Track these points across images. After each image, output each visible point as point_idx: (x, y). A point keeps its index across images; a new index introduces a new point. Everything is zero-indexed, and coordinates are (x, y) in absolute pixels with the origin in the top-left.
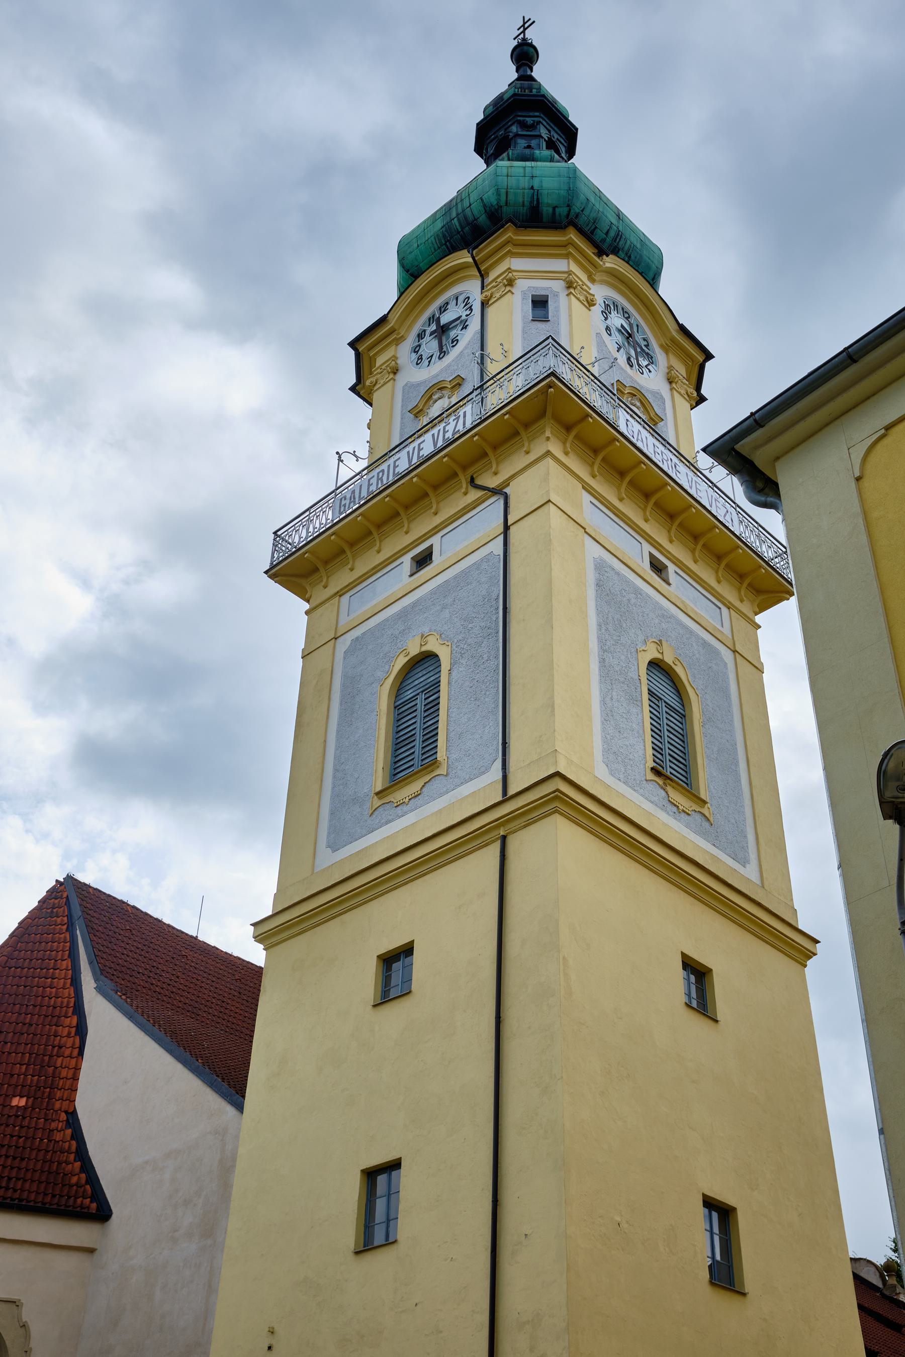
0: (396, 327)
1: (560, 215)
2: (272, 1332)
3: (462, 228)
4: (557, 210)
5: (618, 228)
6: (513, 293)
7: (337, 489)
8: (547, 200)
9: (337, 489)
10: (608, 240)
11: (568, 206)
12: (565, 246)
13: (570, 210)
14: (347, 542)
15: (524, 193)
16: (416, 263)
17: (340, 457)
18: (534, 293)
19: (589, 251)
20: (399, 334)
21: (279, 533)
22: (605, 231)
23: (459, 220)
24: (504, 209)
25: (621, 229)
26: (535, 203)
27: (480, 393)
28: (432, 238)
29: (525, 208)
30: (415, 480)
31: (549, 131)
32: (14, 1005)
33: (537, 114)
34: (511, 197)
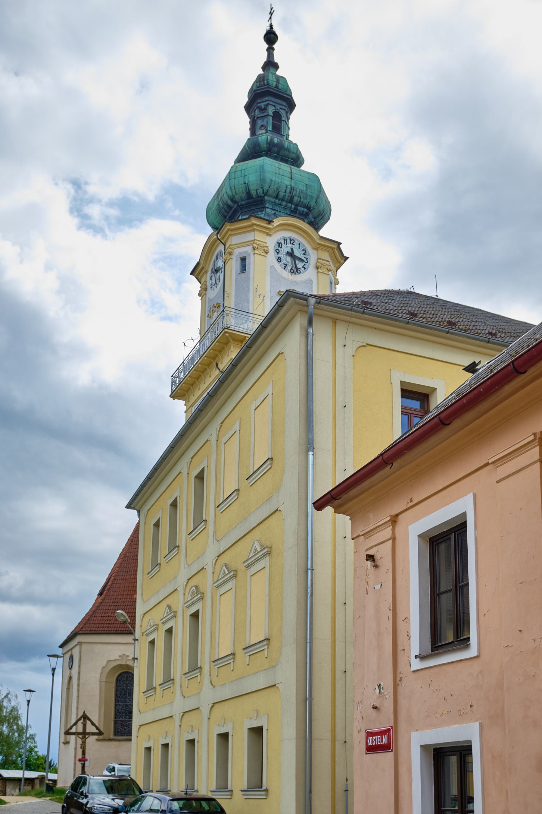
0: (204, 266)
1: (260, 193)
2: (408, 632)
3: (224, 206)
4: (258, 191)
5: (291, 186)
6: (232, 259)
7: (184, 360)
8: (253, 188)
9: (184, 360)
10: (287, 194)
11: (262, 188)
12: (252, 226)
13: (263, 189)
14: (190, 384)
15: (242, 187)
16: (212, 222)
17: (185, 344)
18: (241, 256)
19: (264, 224)
20: (205, 269)
21: (173, 376)
22: (284, 192)
23: (221, 202)
24: (236, 196)
25: (292, 185)
26: (248, 190)
27: (223, 314)
28: (215, 211)
29: (244, 194)
30: (199, 365)
31: (274, 106)
32: (134, 560)
33: (267, 98)
34: (237, 190)
